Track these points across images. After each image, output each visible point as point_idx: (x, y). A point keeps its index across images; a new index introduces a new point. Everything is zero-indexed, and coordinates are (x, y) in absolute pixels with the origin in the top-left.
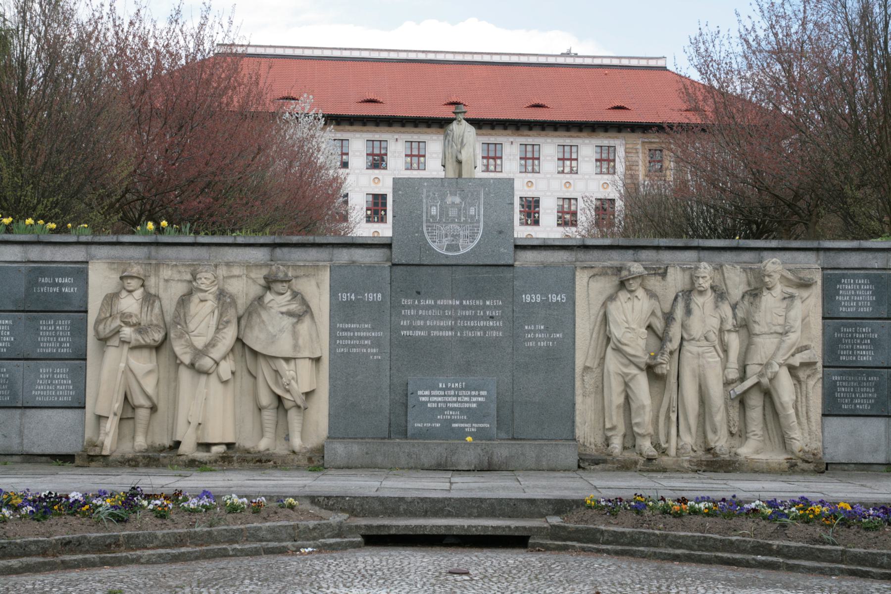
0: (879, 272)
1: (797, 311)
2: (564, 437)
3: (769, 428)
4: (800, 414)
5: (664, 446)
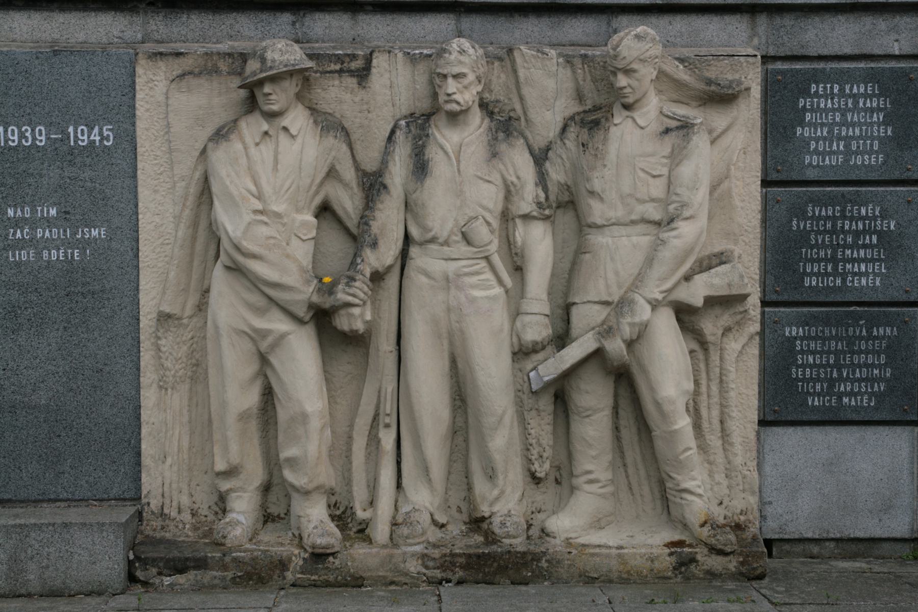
0: (903, 65)
1: (700, 161)
2: (115, 492)
3: (629, 460)
4: (705, 425)
5: (361, 514)
